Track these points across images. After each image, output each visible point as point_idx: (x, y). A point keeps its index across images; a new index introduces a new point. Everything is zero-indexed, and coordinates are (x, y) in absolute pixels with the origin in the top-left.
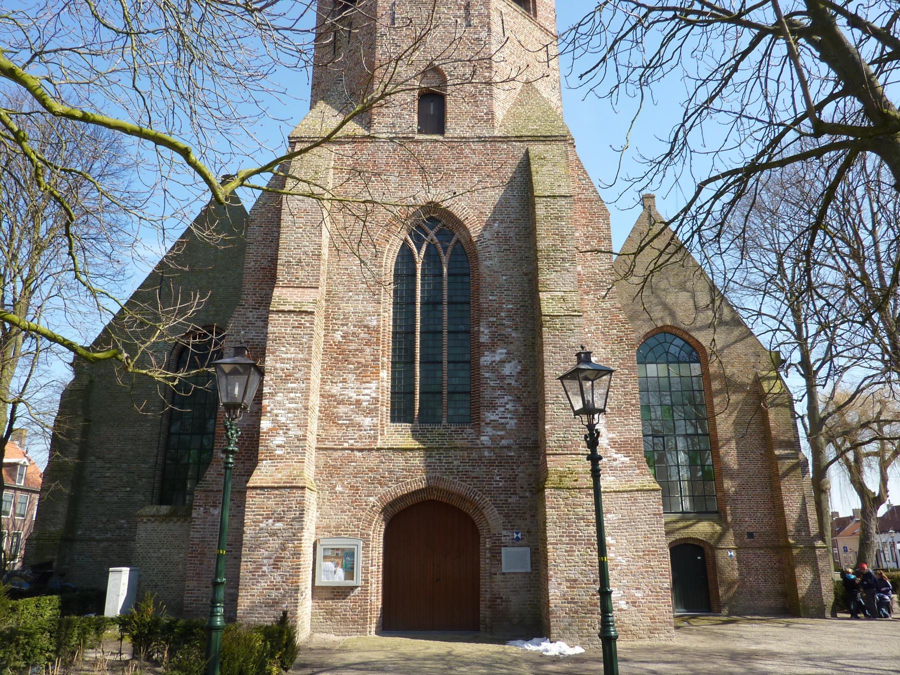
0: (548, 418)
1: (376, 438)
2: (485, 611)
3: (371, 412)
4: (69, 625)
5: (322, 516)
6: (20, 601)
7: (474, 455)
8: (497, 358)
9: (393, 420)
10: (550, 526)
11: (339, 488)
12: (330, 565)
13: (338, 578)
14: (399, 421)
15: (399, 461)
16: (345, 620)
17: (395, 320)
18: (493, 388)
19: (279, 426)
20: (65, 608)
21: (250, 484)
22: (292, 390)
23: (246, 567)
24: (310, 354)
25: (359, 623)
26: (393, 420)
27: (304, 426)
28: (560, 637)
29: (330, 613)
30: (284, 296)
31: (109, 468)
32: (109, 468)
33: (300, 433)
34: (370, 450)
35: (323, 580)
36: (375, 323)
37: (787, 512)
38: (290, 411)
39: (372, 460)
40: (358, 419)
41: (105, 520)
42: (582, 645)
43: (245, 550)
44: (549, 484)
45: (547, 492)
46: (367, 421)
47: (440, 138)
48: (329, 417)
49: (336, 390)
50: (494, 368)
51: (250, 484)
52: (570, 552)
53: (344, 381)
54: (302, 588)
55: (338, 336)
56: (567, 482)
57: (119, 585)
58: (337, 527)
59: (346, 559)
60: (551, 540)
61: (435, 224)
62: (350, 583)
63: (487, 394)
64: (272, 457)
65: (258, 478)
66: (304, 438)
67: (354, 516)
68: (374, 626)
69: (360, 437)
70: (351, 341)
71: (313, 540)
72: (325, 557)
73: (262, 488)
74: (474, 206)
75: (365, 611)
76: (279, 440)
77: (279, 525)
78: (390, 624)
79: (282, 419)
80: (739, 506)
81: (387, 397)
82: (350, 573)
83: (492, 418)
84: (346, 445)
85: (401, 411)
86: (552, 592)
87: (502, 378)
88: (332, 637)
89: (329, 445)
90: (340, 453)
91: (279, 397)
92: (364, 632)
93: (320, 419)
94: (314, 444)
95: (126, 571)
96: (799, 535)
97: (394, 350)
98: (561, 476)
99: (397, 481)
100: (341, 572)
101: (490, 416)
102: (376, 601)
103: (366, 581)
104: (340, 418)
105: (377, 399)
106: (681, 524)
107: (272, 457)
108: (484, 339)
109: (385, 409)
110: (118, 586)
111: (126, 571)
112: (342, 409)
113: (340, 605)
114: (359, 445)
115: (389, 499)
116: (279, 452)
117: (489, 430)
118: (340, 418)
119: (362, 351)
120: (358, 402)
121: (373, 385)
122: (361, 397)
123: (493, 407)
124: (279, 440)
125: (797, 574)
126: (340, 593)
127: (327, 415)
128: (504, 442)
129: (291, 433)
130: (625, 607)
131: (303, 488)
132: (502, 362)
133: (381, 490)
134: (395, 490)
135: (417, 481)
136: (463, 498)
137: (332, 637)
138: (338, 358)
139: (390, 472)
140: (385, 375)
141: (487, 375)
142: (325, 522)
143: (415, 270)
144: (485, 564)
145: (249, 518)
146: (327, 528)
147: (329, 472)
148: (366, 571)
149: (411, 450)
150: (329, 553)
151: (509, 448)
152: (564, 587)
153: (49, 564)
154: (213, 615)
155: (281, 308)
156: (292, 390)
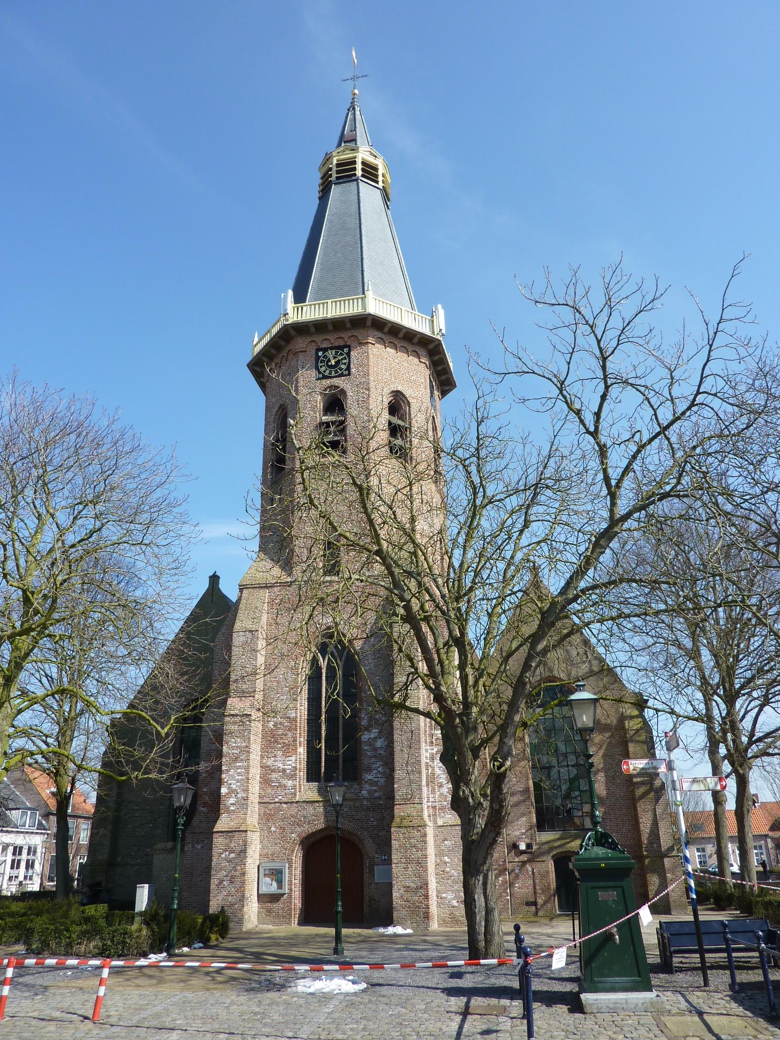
0: (396, 780)
1: (295, 794)
2: (366, 909)
3: (292, 777)
4: (113, 916)
5: (263, 848)
6: (86, 907)
7: (357, 804)
8: (372, 736)
9: (308, 781)
10: (394, 851)
11: (273, 829)
12: (268, 880)
13: (273, 888)
14: (312, 781)
15: (310, 809)
16: (278, 916)
17: (309, 711)
18: (370, 757)
19: (231, 791)
20: (111, 908)
21: (215, 830)
22: (239, 767)
23: (214, 882)
24: (249, 742)
25: (287, 918)
26: (308, 781)
27: (246, 790)
28: (399, 924)
29: (269, 911)
30: (235, 704)
31: (137, 810)
32: (137, 810)
33: (244, 795)
34: (292, 803)
35: (264, 890)
36: (294, 715)
37: (642, 828)
38: (238, 781)
39: (294, 810)
40: (284, 782)
41: (136, 849)
42: (412, 928)
43: (213, 872)
44: (394, 824)
45: (393, 830)
46: (290, 783)
47: (336, 578)
48: (265, 781)
49: (270, 762)
50: (371, 742)
51: (215, 830)
52: (406, 868)
53: (275, 756)
54: (247, 894)
55: (271, 725)
56: (405, 823)
57: (143, 896)
58: (272, 855)
59: (277, 875)
60: (394, 861)
61: (330, 643)
62: (280, 891)
63: (366, 761)
64: (228, 811)
65: (220, 825)
66: (246, 799)
67: (283, 847)
68: (296, 919)
69: (286, 794)
70: (279, 728)
71: (258, 863)
72: (265, 875)
73: (222, 832)
74: (354, 629)
75: (290, 910)
76: (232, 801)
77: (232, 855)
78: (305, 920)
79: (234, 787)
80: (608, 824)
81: (304, 765)
82: (280, 884)
83: (369, 778)
84: (277, 800)
85: (313, 774)
86: (394, 894)
87: (376, 749)
88: (270, 927)
89: (266, 800)
90: (273, 805)
91: (232, 772)
92: (290, 923)
93: (260, 782)
94: (257, 800)
95: (146, 886)
96: (652, 847)
97: (308, 732)
98: (402, 819)
99: (309, 823)
100: (275, 884)
101: (368, 777)
102: (297, 902)
103: (291, 890)
104: (273, 782)
105: (295, 768)
106: (559, 843)
107: (228, 811)
108: (364, 723)
109: (302, 774)
110: (142, 896)
111: (146, 886)
112: (274, 776)
113: (276, 906)
114: (285, 800)
115: (304, 835)
116: (232, 808)
117: (367, 786)
118: (273, 782)
119: (286, 735)
120: (284, 770)
121: (293, 758)
122: (286, 767)
123: (369, 770)
124: (232, 801)
125: (649, 879)
126: (274, 898)
127: (265, 780)
128: (377, 794)
129: (239, 796)
130: (456, 904)
131: (246, 831)
132: (375, 738)
133: (298, 829)
134: (308, 829)
135: (320, 824)
136: (351, 833)
137: (270, 927)
138: (271, 741)
139: (305, 817)
140: (302, 750)
141: (366, 748)
142: (265, 851)
143: (321, 673)
144: (366, 877)
145: (215, 852)
146: (266, 856)
147: (266, 818)
148: (290, 882)
149: (317, 802)
150: (267, 872)
151: (379, 798)
152: (402, 891)
153: (99, 884)
154: (173, 904)
155: (232, 712)
156: (239, 767)
